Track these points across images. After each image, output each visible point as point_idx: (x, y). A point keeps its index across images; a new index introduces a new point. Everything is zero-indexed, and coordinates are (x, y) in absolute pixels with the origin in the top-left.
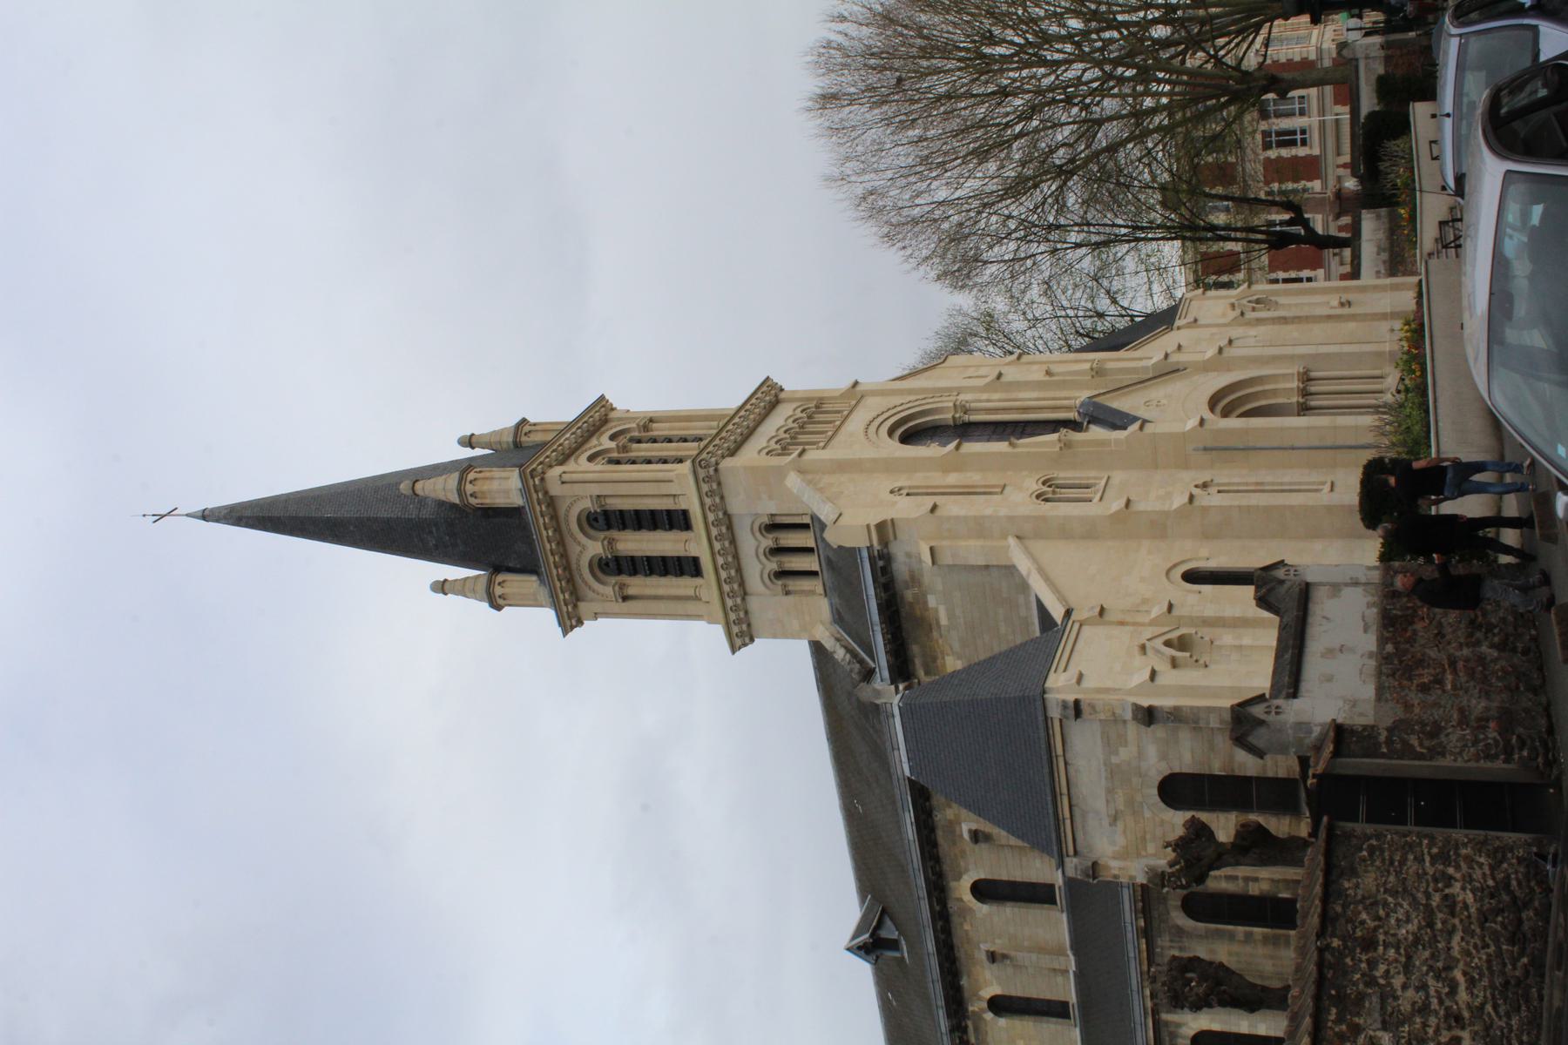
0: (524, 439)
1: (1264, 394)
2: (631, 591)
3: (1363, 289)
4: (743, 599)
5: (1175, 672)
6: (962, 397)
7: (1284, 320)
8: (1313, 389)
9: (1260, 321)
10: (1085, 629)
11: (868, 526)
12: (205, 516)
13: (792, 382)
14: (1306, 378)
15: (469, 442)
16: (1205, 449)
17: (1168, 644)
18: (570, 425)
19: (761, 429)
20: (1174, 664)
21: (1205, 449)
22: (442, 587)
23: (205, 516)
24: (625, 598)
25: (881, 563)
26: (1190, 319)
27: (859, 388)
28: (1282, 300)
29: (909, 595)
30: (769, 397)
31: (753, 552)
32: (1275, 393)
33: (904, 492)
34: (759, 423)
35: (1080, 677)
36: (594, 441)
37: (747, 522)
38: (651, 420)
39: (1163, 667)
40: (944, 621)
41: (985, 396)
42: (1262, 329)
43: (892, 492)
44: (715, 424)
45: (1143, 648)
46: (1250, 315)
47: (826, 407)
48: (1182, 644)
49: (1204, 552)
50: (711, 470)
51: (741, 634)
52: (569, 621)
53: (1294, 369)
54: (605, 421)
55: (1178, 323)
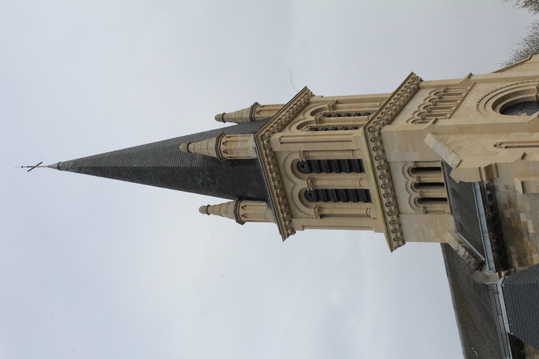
0: (257, 116)
2: (325, 212)
4: (398, 216)
12: (60, 167)
15: (222, 118)
19: (408, 107)
22: (206, 210)
23: (60, 167)
25: (488, 193)
27: (472, 78)
29: (507, 213)
33: (504, 146)
34: (407, 102)
36: (301, 116)
38: (337, 102)
40: (531, 230)
47: (451, 91)
50: (376, 134)
51: (397, 239)
52: (286, 231)
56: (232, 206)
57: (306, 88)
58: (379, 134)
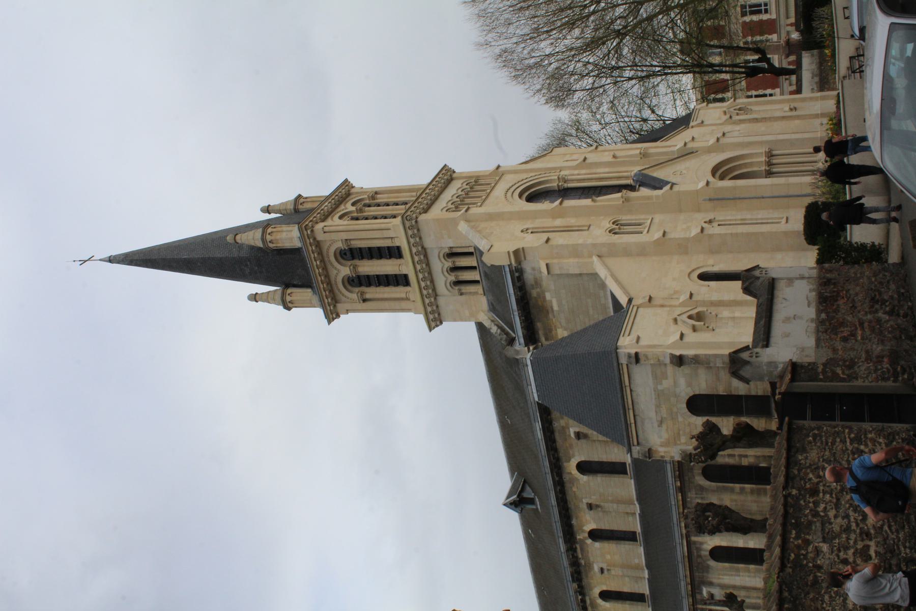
0: (300, 207)
1: (745, 165)
2: (368, 296)
3: (803, 100)
4: (435, 299)
5: (695, 334)
6: (563, 173)
7: (756, 120)
8: (774, 161)
9: (742, 121)
10: (641, 310)
11: (509, 252)
12: (111, 260)
13: (459, 167)
14: (770, 155)
15: (267, 210)
16: (710, 200)
17: (690, 317)
18: (328, 198)
19: (442, 196)
20: (694, 329)
21: (710, 200)
22: (254, 298)
23: (111, 260)
24: (364, 300)
25: (517, 274)
26: (699, 121)
27: (500, 169)
28: (754, 108)
29: (534, 293)
30: (446, 177)
31: (440, 271)
32: (751, 164)
33: (530, 231)
35: (638, 338)
36: (342, 207)
37: (436, 252)
38: (376, 193)
39: (687, 331)
40: (556, 308)
41: (576, 172)
42: (743, 126)
43: (522, 231)
44: (414, 194)
45: (675, 320)
46: (736, 118)
48: (699, 317)
49: (711, 262)
50: (413, 222)
51: (435, 320)
52: (332, 315)
53: (763, 149)
54: (348, 194)
55: (692, 124)
56: (279, 293)
57: (346, 180)
58: (416, 222)
